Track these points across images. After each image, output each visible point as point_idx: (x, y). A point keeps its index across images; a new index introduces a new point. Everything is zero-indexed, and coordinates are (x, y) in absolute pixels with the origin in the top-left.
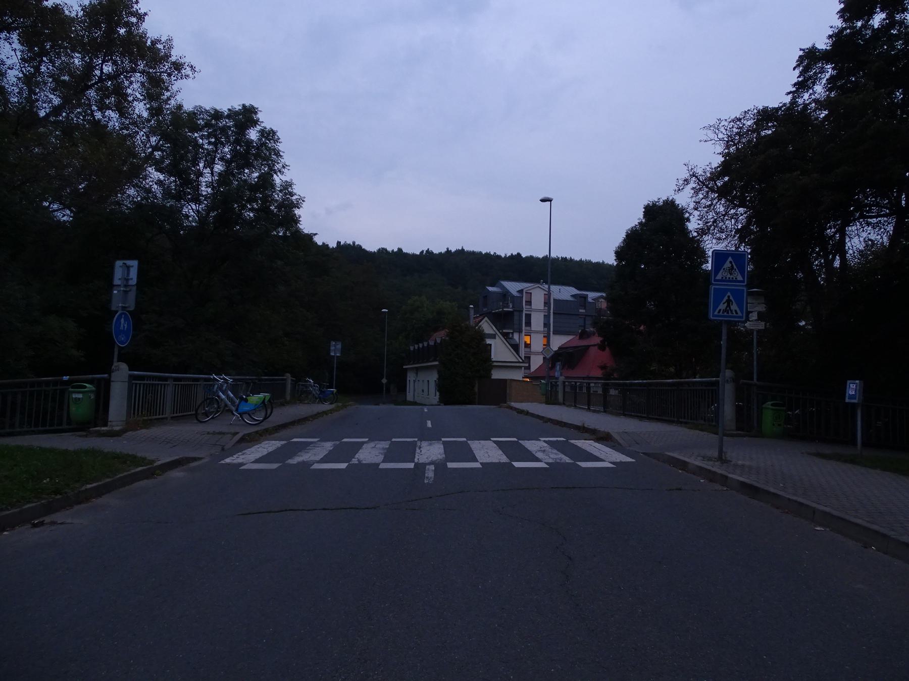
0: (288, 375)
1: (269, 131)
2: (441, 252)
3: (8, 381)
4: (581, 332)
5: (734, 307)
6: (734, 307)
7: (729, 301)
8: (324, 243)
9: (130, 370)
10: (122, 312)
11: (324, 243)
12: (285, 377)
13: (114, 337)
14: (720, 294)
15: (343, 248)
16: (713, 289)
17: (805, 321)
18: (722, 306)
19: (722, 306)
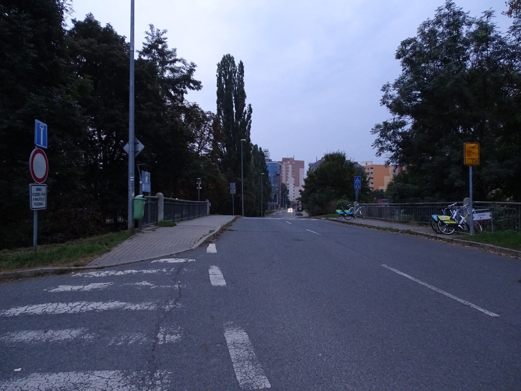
0: (207, 201)
1: (493, 217)
2: (204, 111)
3: (192, 201)
4: (236, 190)
5: (359, 186)
6: (359, 186)
7: (358, 185)
8: (109, 25)
9: (164, 197)
10: (37, 149)
11: (109, 25)
12: (206, 202)
13: (32, 176)
14: (356, 184)
15: (218, 86)
16: (138, 166)
17: (304, 191)
18: (357, 186)
19: (357, 186)
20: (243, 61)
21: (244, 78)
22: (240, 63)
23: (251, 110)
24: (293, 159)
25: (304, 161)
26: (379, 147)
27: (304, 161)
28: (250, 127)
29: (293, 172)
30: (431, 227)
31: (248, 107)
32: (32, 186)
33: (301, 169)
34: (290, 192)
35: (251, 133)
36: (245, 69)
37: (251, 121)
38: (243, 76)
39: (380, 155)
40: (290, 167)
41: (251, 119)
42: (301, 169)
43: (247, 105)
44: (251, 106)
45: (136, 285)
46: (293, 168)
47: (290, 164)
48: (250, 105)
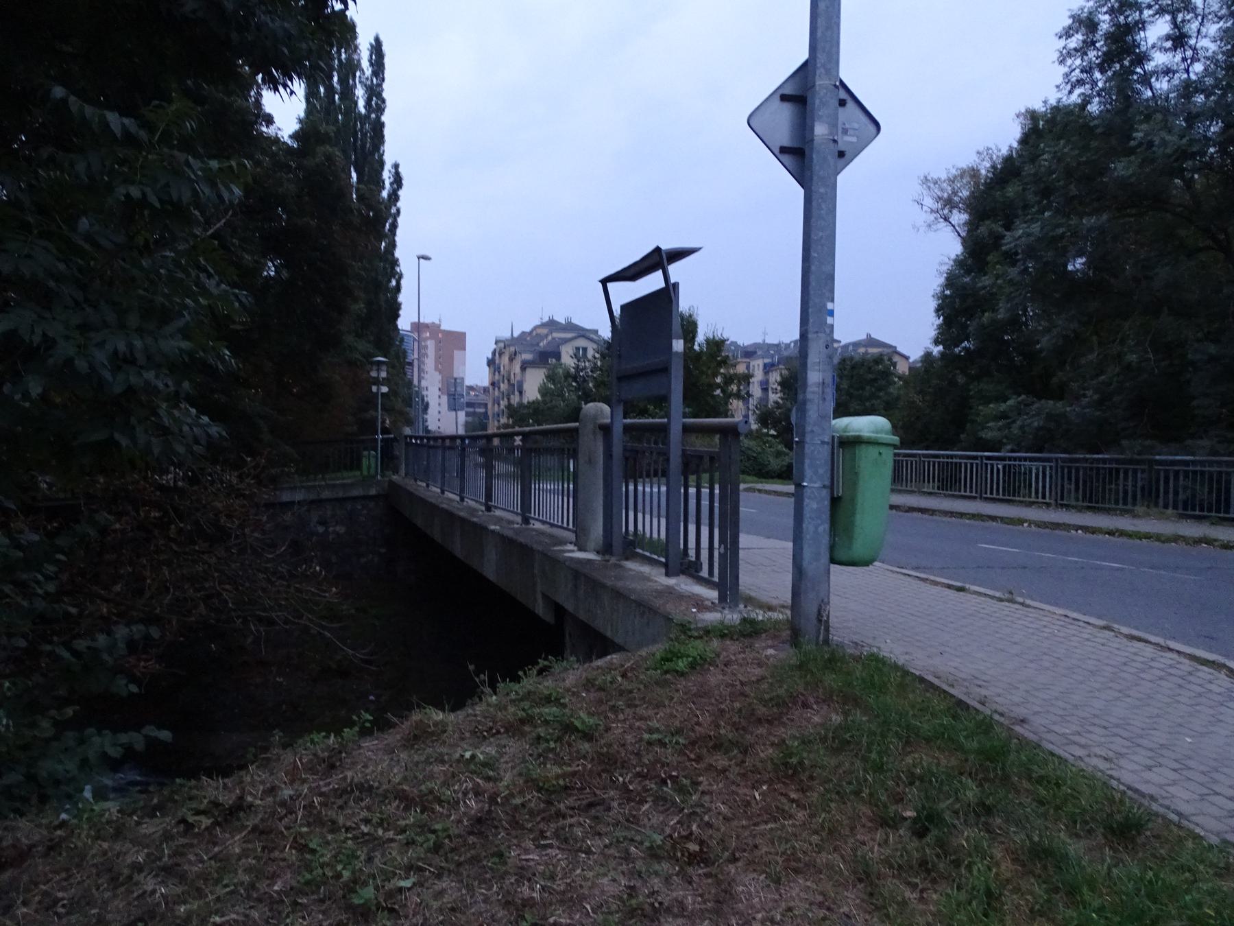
20: (382, 38)
21: (385, 86)
22: (373, 42)
23: (398, 181)
24: (439, 326)
25: (463, 335)
26: (1190, 47)
27: (463, 335)
28: (394, 226)
29: (438, 358)
30: (790, 545)
31: (390, 172)
32: (610, 285)
33: (457, 353)
34: (430, 411)
35: (398, 244)
36: (387, 61)
37: (398, 211)
38: (383, 80)
39: (1060, 37)
40: (431, 344)
41: (399, 204)
42: (457, 353)
43: (388, 167)
44: (400, 170)
45: (1180, 96)
46: (438, 349)
47: (430, 338)
48: (396, 166)
